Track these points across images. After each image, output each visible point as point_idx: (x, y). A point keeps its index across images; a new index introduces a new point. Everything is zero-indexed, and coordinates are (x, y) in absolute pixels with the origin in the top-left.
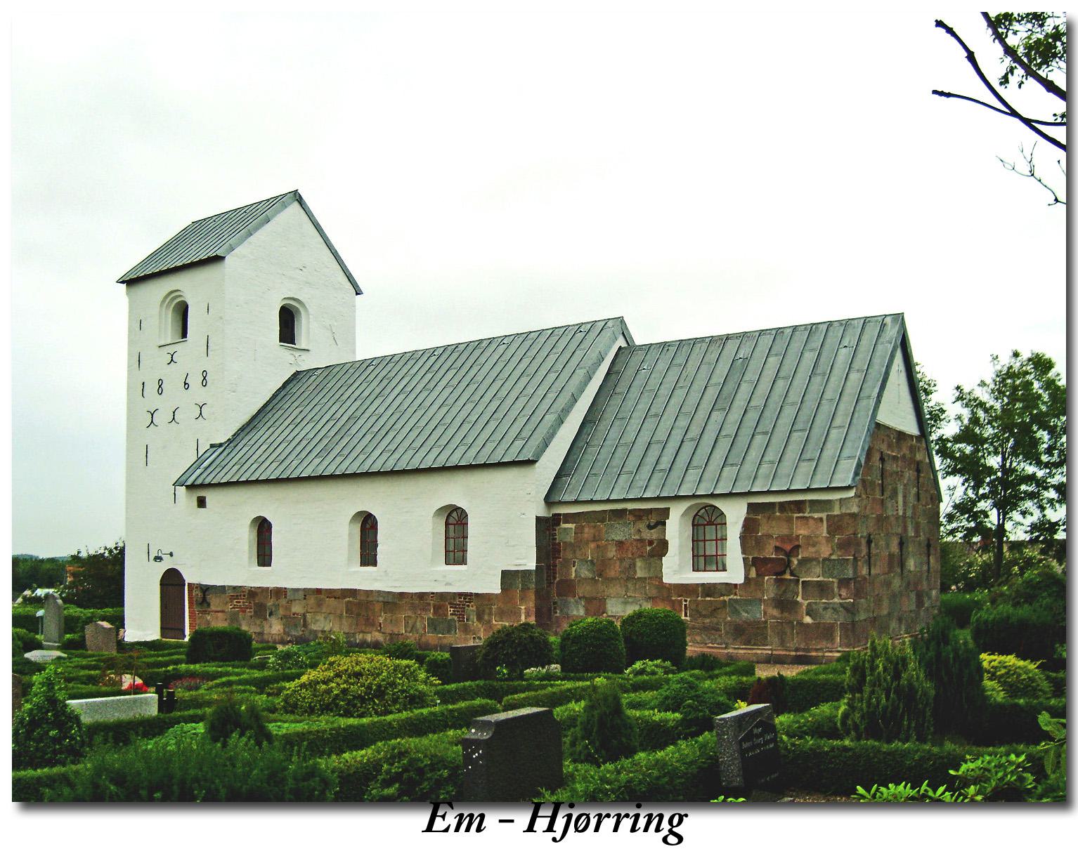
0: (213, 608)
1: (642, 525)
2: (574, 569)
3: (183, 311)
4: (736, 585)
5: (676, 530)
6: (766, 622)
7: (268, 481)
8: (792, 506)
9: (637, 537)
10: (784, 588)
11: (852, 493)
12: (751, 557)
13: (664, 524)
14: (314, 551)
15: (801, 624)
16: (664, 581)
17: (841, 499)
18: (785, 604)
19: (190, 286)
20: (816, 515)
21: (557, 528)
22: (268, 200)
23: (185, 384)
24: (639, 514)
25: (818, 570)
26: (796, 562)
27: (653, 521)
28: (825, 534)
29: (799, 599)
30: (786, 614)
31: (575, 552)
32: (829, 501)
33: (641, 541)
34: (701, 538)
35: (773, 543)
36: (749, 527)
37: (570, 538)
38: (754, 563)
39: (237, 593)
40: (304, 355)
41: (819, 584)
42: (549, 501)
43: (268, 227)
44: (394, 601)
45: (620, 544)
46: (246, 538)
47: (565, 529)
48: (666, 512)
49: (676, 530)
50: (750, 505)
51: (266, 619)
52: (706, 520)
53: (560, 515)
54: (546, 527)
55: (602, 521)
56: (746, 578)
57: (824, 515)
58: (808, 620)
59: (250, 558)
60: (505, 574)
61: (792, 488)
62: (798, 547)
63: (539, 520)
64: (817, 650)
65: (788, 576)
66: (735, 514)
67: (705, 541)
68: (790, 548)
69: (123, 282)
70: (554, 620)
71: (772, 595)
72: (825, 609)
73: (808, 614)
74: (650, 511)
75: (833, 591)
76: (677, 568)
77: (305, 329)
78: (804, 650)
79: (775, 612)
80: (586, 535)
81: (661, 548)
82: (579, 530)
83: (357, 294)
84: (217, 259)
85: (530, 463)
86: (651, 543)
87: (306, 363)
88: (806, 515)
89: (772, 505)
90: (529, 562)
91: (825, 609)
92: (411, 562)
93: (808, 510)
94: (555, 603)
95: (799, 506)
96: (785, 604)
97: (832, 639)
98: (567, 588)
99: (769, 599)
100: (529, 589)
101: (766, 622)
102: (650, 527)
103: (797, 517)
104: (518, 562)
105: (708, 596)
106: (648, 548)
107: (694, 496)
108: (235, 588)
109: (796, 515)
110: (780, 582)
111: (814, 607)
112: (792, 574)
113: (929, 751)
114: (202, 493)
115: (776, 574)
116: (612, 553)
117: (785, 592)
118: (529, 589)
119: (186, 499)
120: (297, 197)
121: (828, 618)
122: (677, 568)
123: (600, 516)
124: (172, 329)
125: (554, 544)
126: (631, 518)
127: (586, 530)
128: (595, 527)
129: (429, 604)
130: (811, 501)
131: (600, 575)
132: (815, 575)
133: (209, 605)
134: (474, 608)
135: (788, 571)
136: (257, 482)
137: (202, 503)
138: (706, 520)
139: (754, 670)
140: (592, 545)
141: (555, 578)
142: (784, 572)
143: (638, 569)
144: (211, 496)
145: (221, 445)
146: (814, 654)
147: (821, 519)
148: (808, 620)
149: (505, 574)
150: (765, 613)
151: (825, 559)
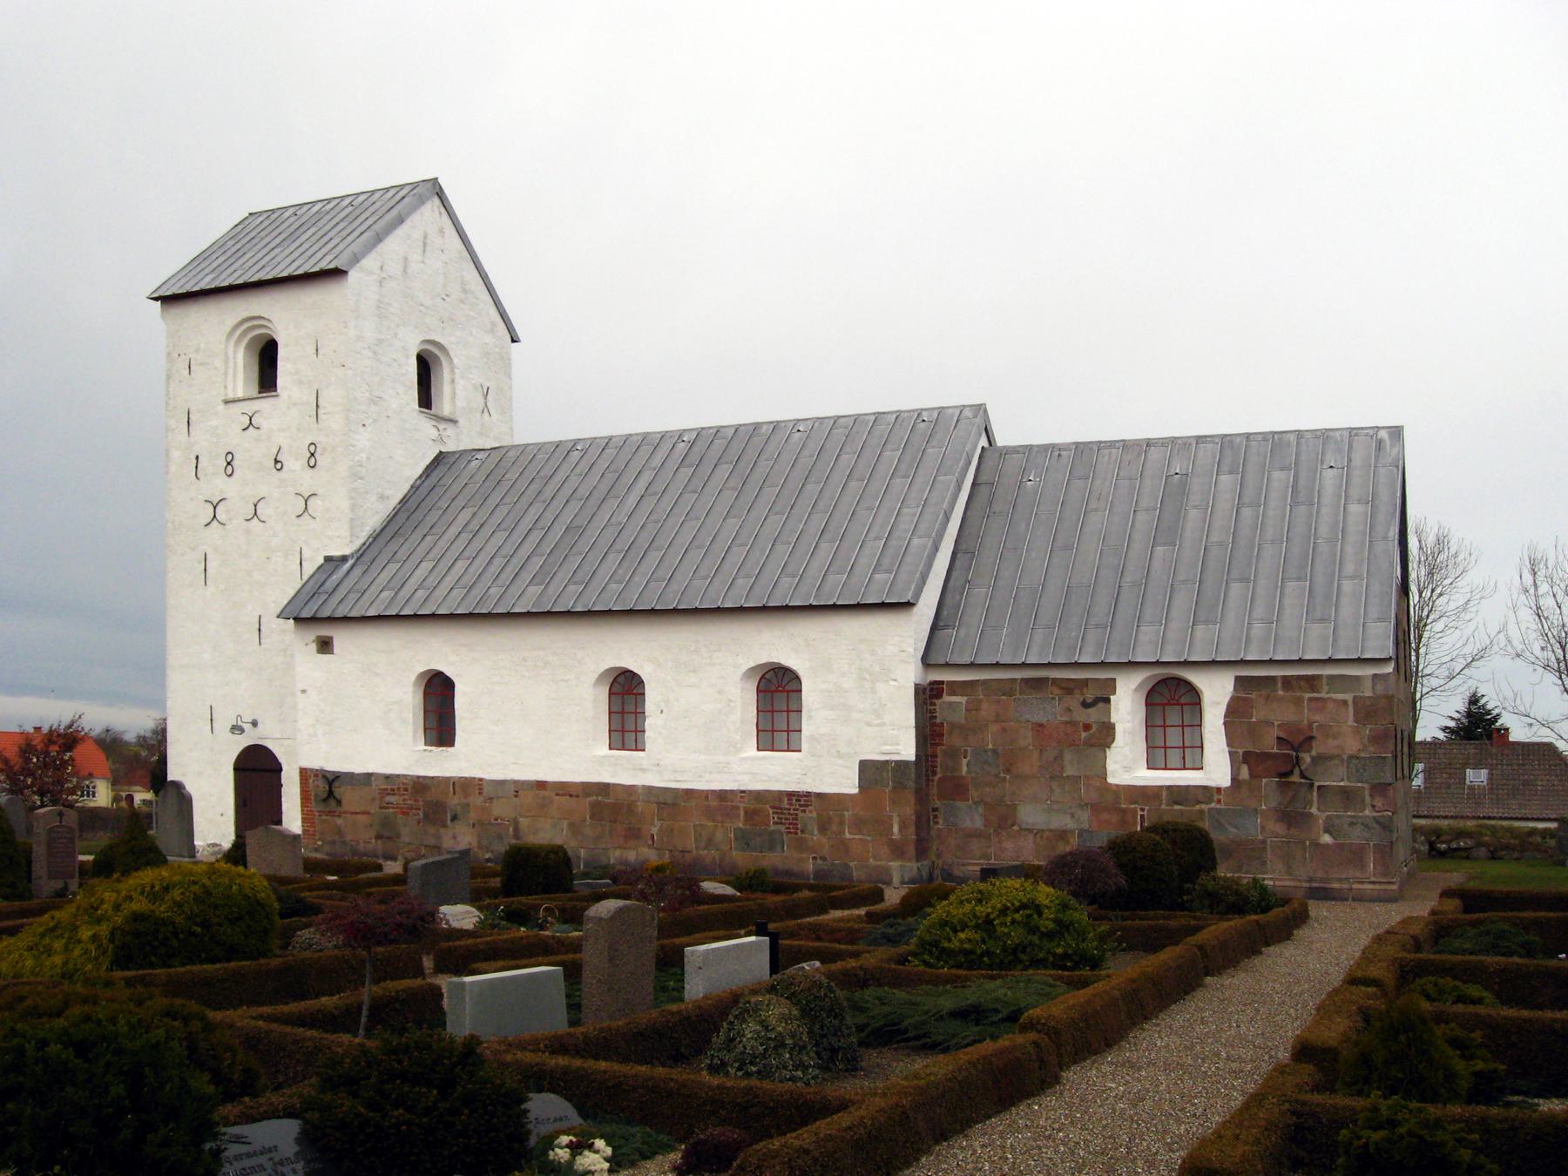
0: (345, 806)
1: (1074, 702)
2: (965, 761)
3: (267, 357)
4: (1219, 790)
5: (1126, 708)
6: (1264, 842)
7: (452, 617)
8: (1302, 683)
9: (1064, 719)
10: (1291, 794)
11: (1389, 668)
12: (1241, 751)
13: (1108, 701)
14: (530, 724)
15: (1316, 845)
16: (1110, 780)
17: (1375, 675)
18: (1292, 817)
19: (285, 316)
20: (1340, 696)
21: (938, 702)
22: (387, 190)
23: (276, 461)
24: (1068, 687)
25: (1342, 771)
26: (1308, 760)
27: (1090, 697)
28: (1351, 721)
29: (1314, 810)
30: (1294, 831)
31: (966, 738)
32: (1357, 678)
33: (1073, 723)
34: (1160, 722)
35: (1275, 732)
36: (1235, 712)
37: (960, 717)
38: (1245, 758)
39: (392, 784)
40: (450, 430)
41: (1344, 792)
42: (927, 662)
43: (401, 231)
44: (673, 802)
45: (1039, 727)
46: (409, 701)
47: (950, 704)
48: (1111, 685)
49: (1126, 708)
50: (1238, 679)
51: (445, 826)
52: (1171, 698)
53: (942, 682)
54: (927, 696)
55: (1010, 694)
56: (1234, 779)
57: (1349, 697)
58: (1327, 839)
59: (415, 732)
60: (865, 766)
61: (1306, 657)
62: (1311, 738)
63: (917, 687)
64: (1340, 880)
65: (1295, 778)
66: (1216, 692)
67: (1164, 726)
68: (1296, 742)
69: (156, 299)
70: (933, 833)
71: (1273, 805)
72: (1352, 824)
73: (1327, 831)
74: (1086, 682)
75: (1363, 800)
76: (1127, 764)
77: (453, 390)
78: (1322, 880)
79: (1279, 828)
80: (983, 713)
81: (1105, 734)
82: (972, 708)
83: (513, 341)
84: (336, 273)
85: (908, 605)
86: (1087, 727)
87: (454, 442)
88: (1323, 695)
89: (1271, 680)
90: (906, 749)
91: (1352, 824)
92: (700, 741)
93: (1326, 688)
94: (935, 810)
95: (1312, 682)
96: (1292, 817)
97: (1363, 867)
98: (956, 789)
99: (1269, 809)
100: (905, 788)
101: (1264, 842)
102: (1085, 705)
103: (1310, 699)
104: (888, 748)
105: (1176, 803)
106: (1084, 735)
107: (1158, 663)
108: (388, 777)
109: (1307, 695)
110: (1284, 786)
111: (1337, 821)
112: (1303, 776)
113: (362, 1045)
114: (325, 631)
115: (1281, 775)
116: (1026, 739)
117: (1293, 799)
118: (905, 788)
119: (300, 644)
120: (435, 190)
121: (1356, 836)
122: (1127, 764)
123: (1007, 688)
124: (246, 379)
125: (934, 725)
126: (1057, 691)
127: (985, 706)
128: (998, 702)
129: (737, 808)
130: (1331, 677)
131: (1008, 771)
132: (1336, 778)
133: (339, 802)
134: (814, 815)
135: (1297, 771)
136: (433, 617)
137: (325, 646)
138: (1171, 698)
139: (1306, 911)
140: (993, 728)
141: (934, 773)
142: (1291, 773)
143: (1067, 763)
144: (343, 639)
145: (344, 559)
146: (1336, 885)
147: (1345, 702)
148: (1327, 839)
149: (865, 766)
150: (1263, 828)
151: (1351, 757)
